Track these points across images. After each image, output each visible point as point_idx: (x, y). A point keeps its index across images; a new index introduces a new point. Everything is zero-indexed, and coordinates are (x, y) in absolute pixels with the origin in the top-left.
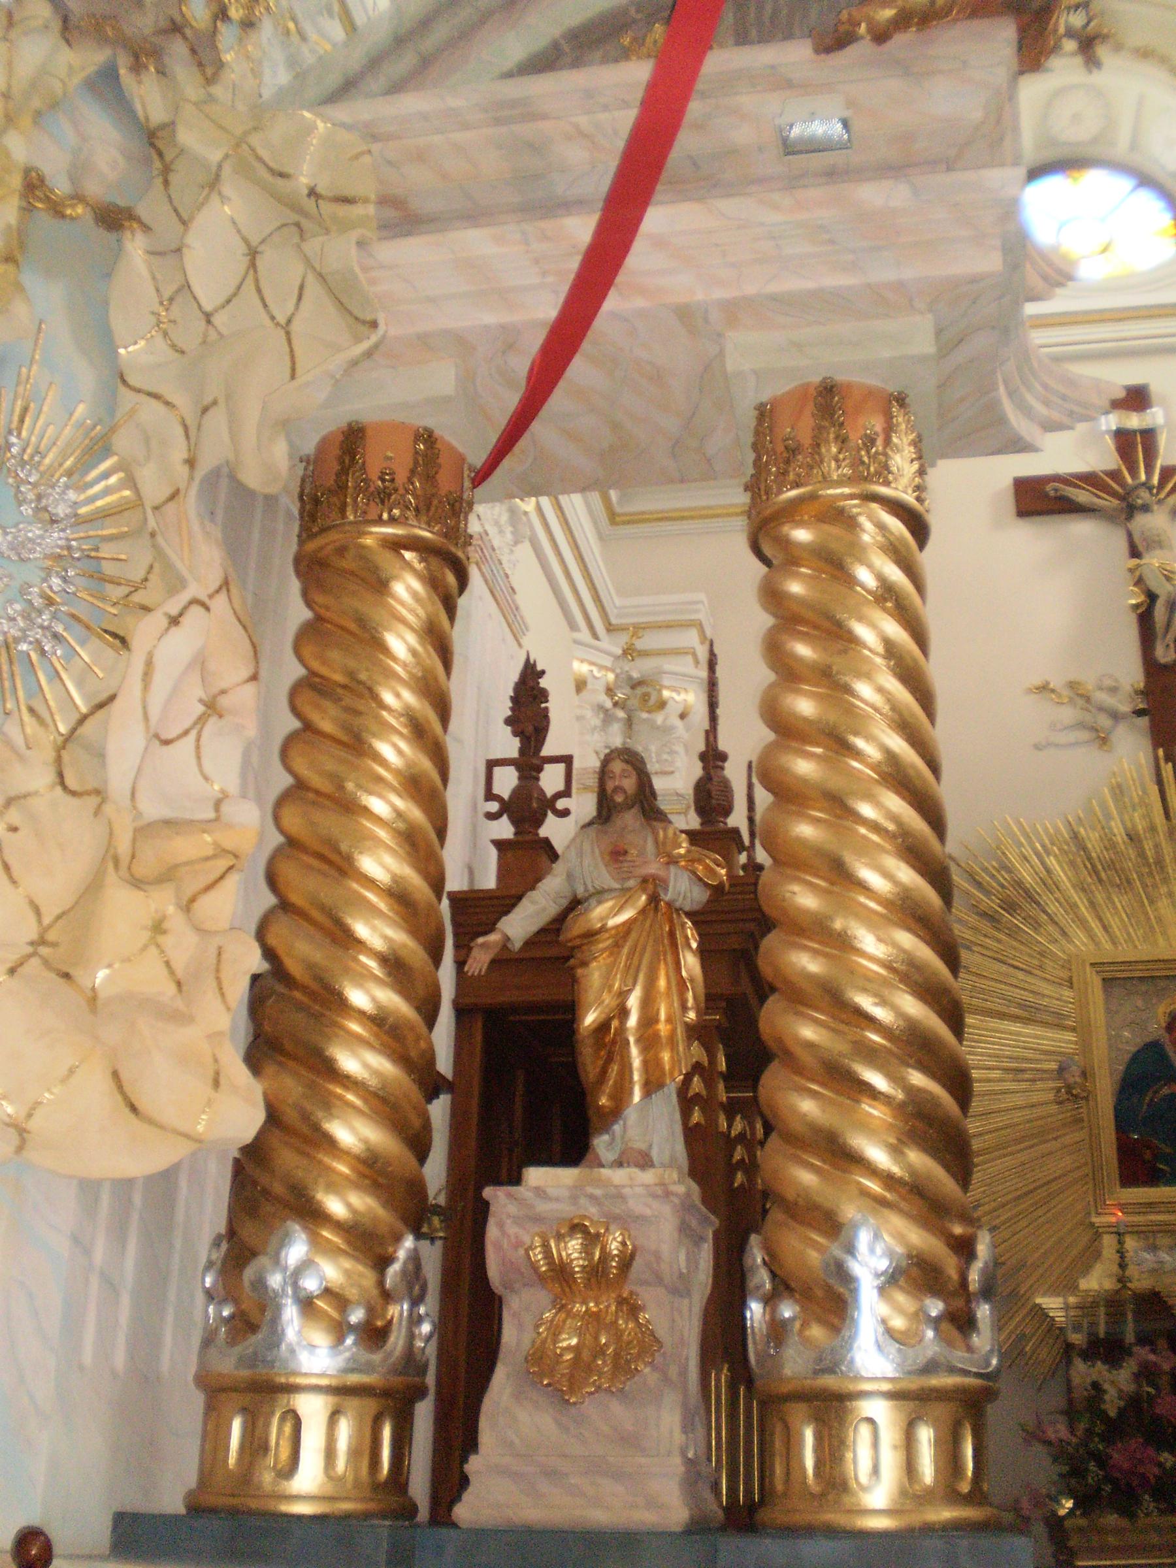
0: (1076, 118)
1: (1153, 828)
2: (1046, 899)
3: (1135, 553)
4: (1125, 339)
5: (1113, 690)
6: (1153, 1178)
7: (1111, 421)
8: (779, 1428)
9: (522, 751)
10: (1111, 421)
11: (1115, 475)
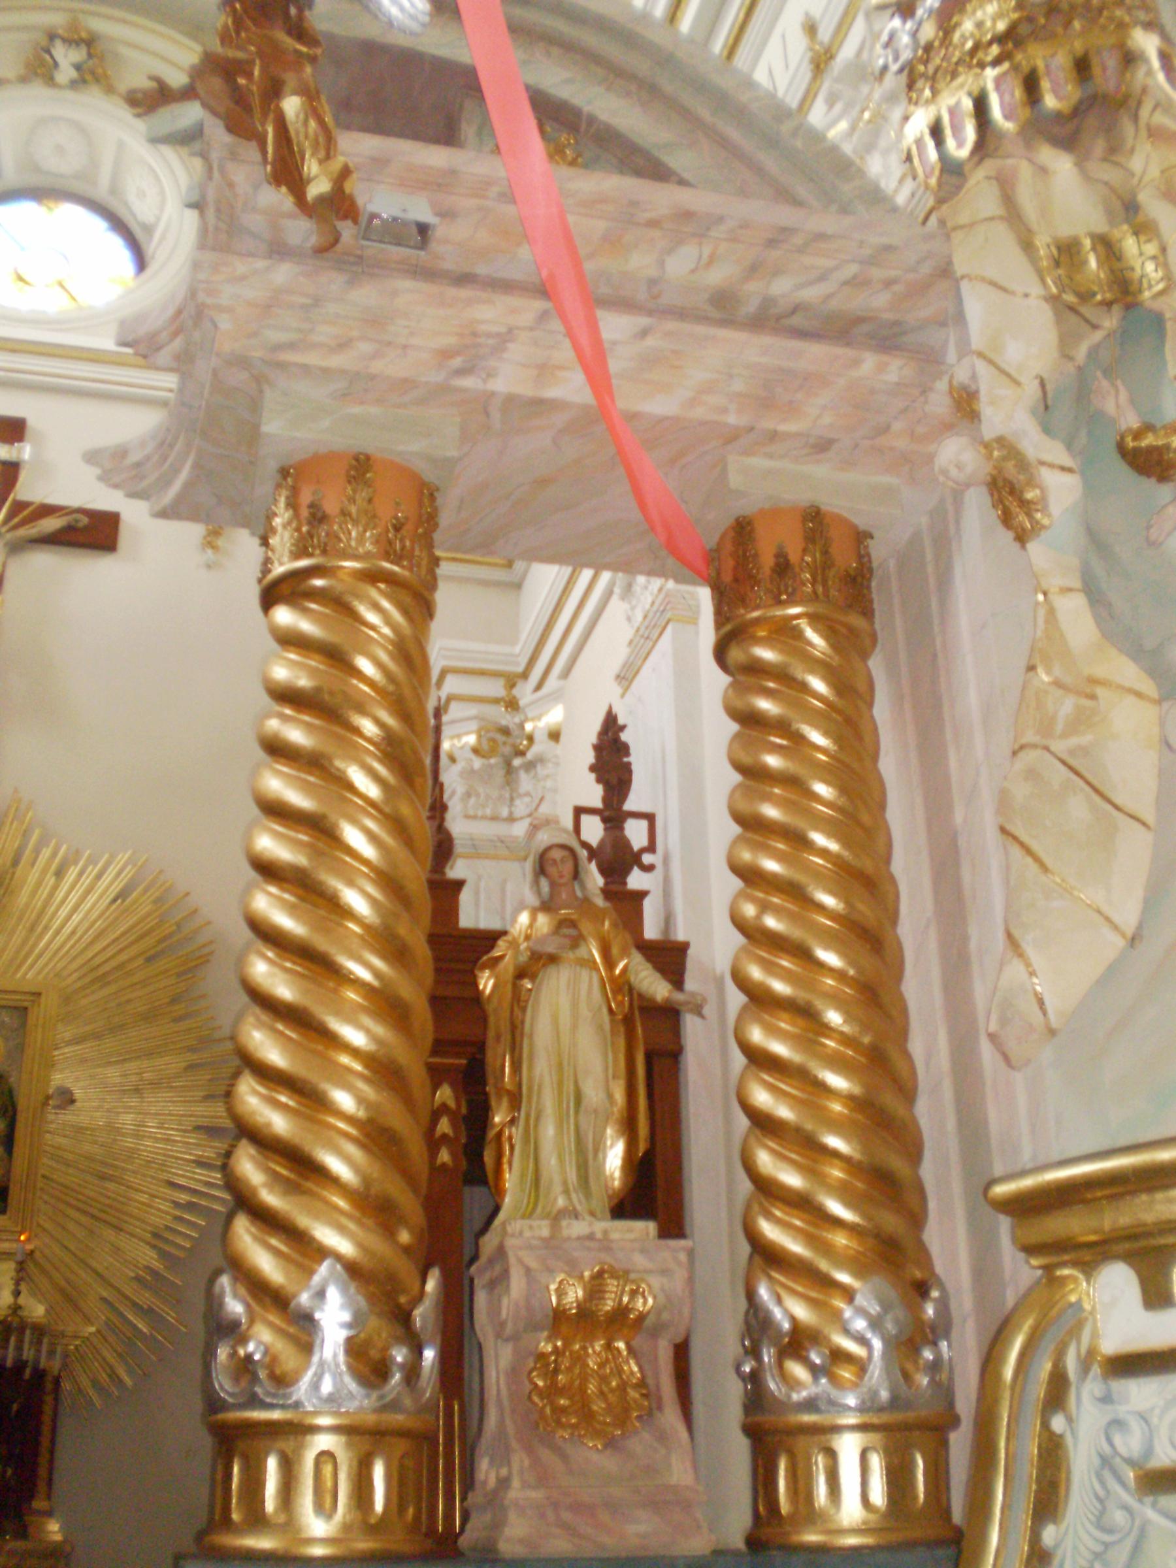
0: (60, 150)
4: (18, 371)
8: (820, 1460)
9: (606, 800)
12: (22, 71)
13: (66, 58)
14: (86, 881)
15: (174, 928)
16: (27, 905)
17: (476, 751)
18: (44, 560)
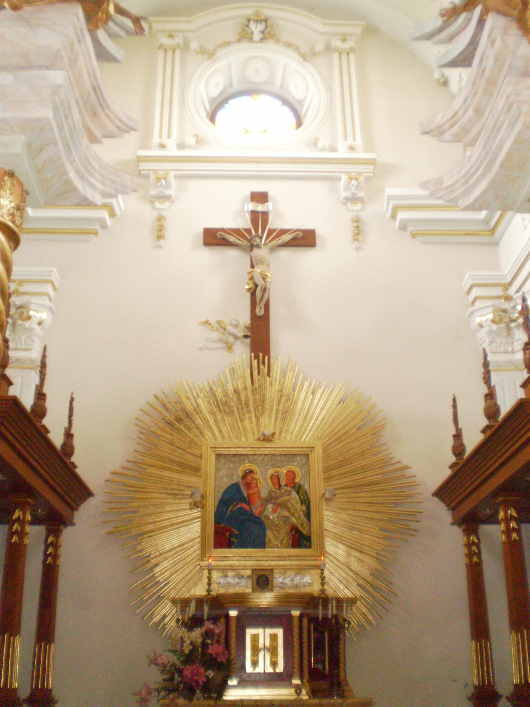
1: (246, 388)
2: (196, 416)
3: (252, 266)
5: (236, 326)
6: (229, 545)
7: (251, 206)
10: (251, 206)
11: (248, 231)
12: (238, 37)
13: (256, 29)
14: (325, 396)
15: (367, 414)
16: (301, 409)
17: (493, 321)
18: (285, 254)
